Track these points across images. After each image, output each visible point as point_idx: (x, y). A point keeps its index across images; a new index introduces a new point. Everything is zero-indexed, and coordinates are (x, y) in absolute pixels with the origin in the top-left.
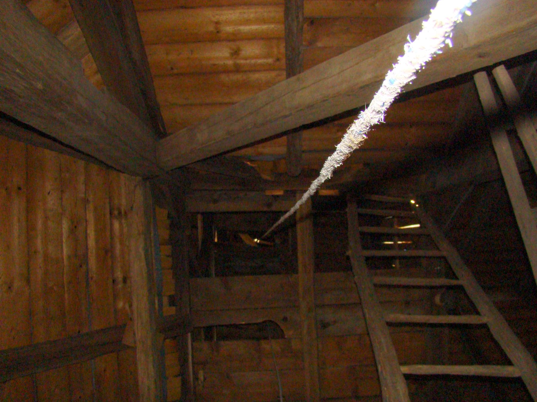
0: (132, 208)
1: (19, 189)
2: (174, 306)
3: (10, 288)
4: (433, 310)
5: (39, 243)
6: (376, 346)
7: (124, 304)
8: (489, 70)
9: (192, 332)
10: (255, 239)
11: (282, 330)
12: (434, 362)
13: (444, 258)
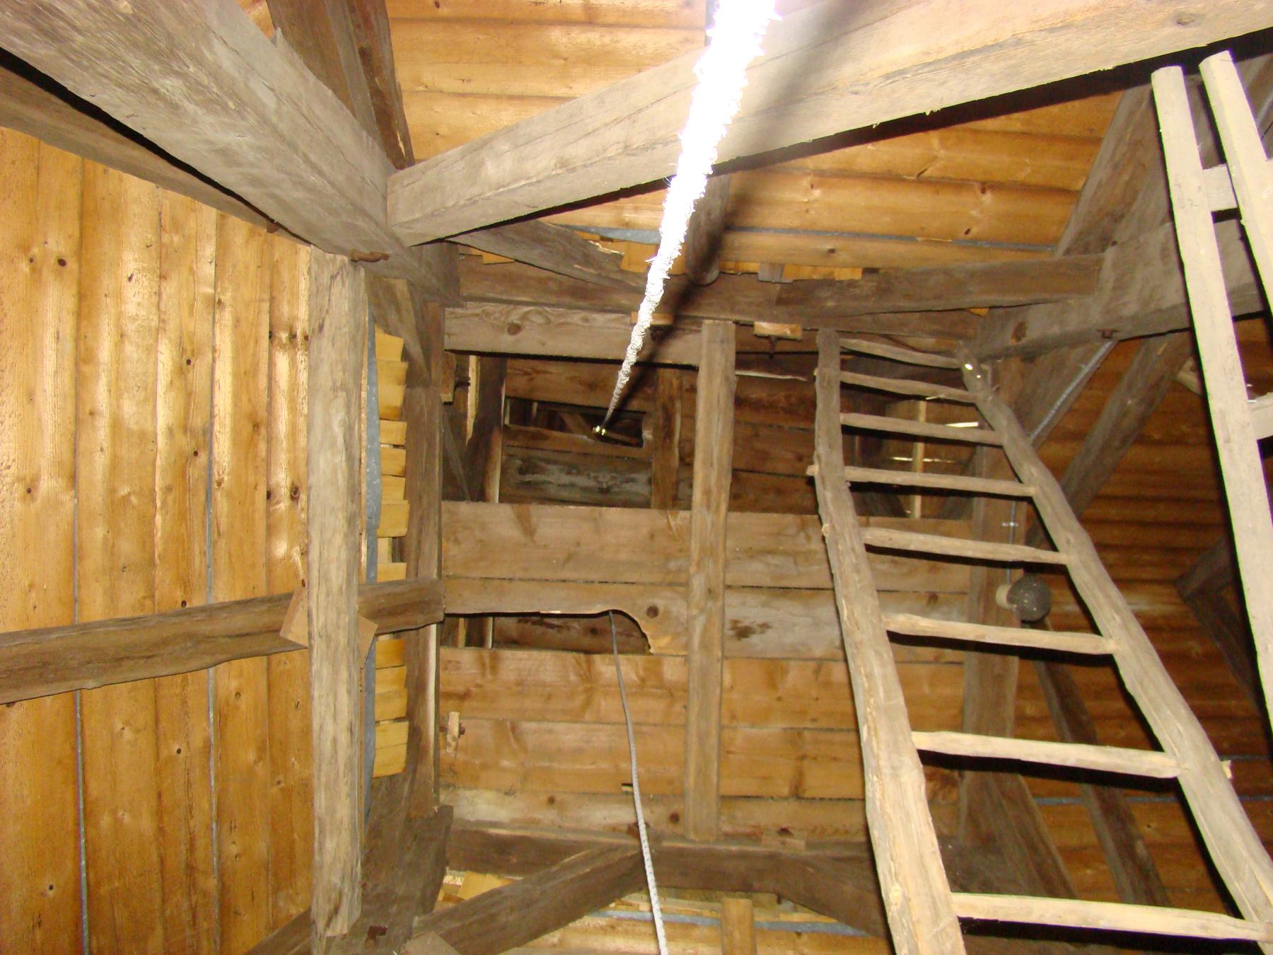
0: (321, 328)
1: (62, 263)
2: (402, 561)
3: (29, 491)
4: (989, 614)
5: (101, 395)
6: (860, 684)
7: (291, 547)
8: (1190, 61)
9: (440, 623)
10: (596, 427)
11: (644, 636)
12: (981, 729)
13: (1029, 500)
